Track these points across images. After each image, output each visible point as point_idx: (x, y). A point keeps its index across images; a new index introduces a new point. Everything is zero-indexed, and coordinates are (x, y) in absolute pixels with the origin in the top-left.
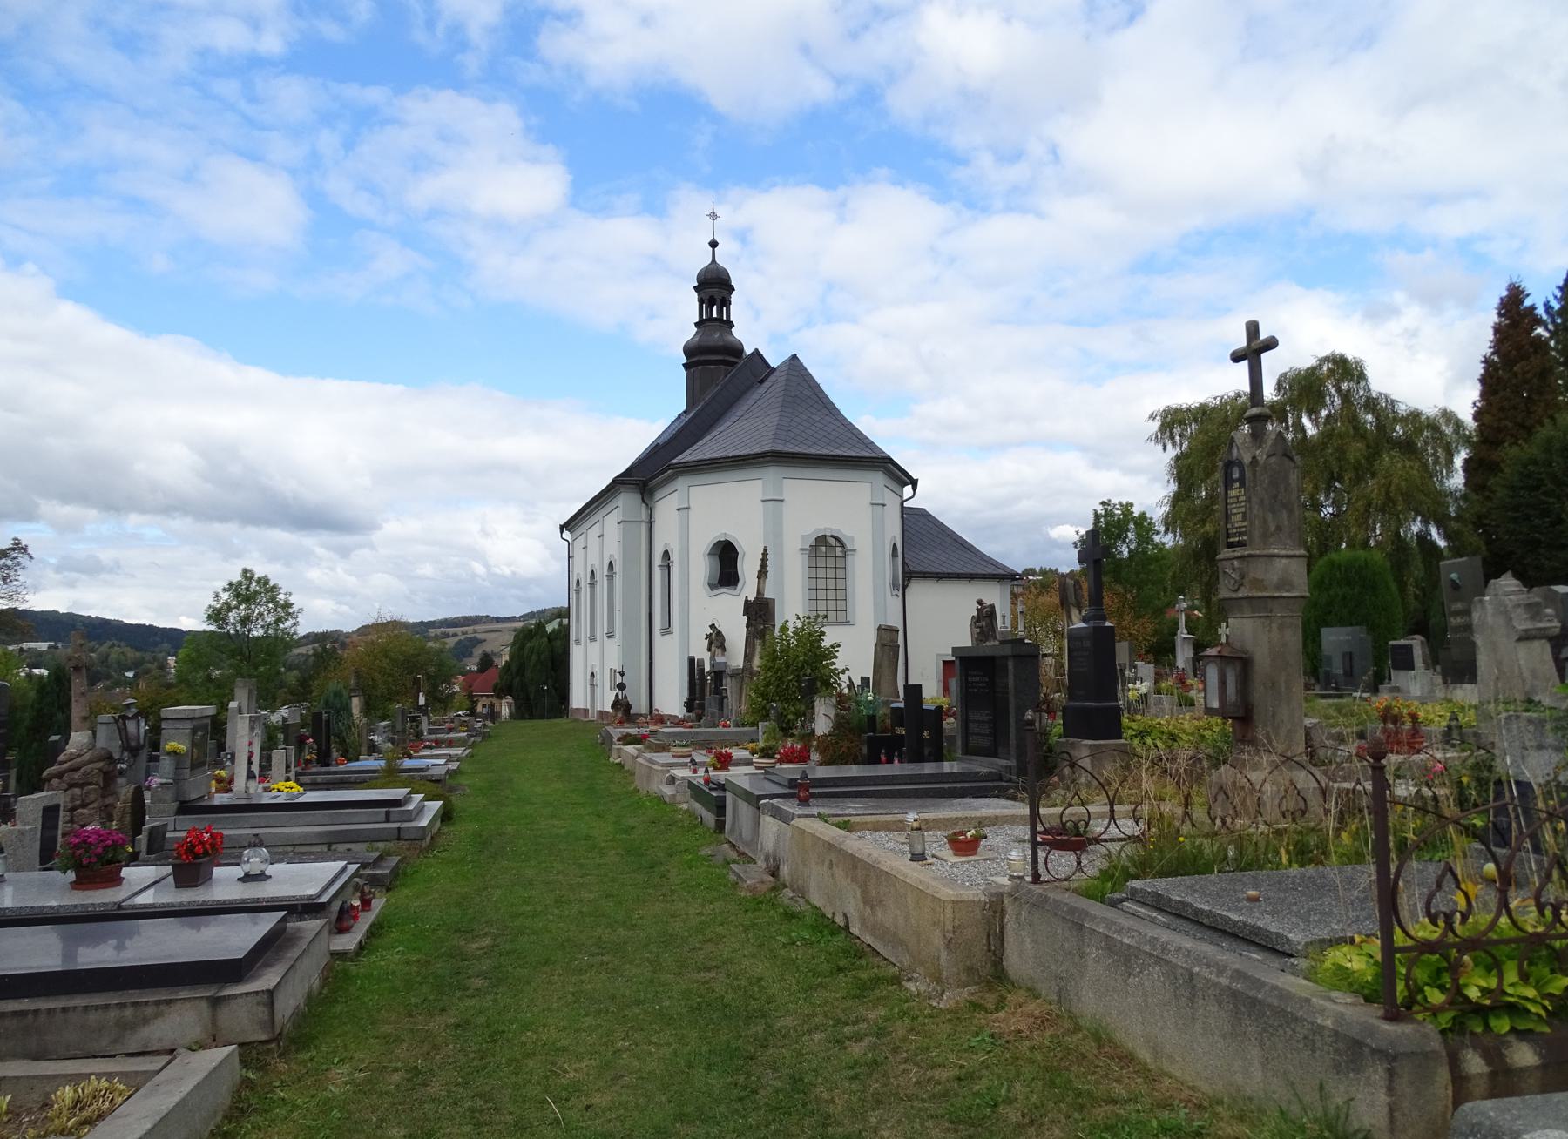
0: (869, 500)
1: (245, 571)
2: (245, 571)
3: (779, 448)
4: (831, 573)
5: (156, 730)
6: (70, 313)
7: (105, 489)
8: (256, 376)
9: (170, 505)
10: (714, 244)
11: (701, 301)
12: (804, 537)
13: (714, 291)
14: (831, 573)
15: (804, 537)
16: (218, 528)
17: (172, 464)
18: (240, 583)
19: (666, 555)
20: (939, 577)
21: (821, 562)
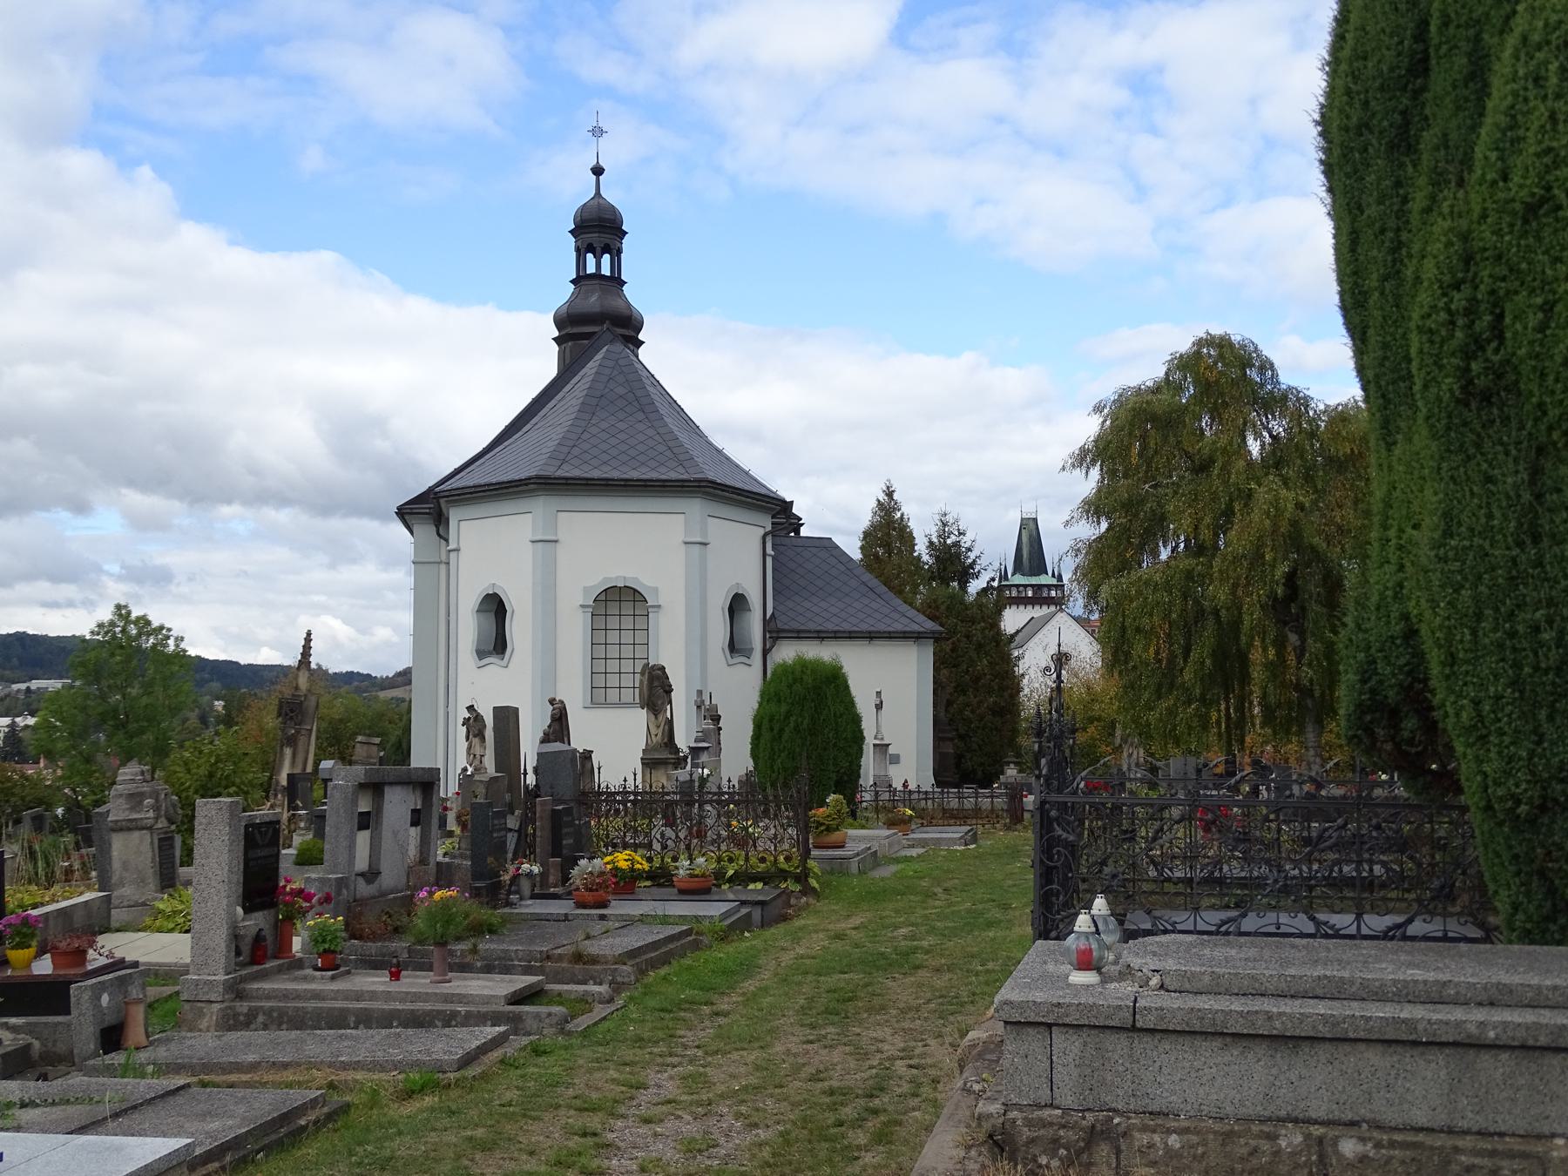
0: (681, 538)
1: (119, 607)
2: (119, 607)
3: (550, 471)
4: (627, 637)
5: (1530, 759)
6: (195, 237)
7: (189, 475)
8: (419, 309)
9: (267, 494)
10: (598, 171)
11: (578, 250)
12: (586, 590)
13: (593, 237)
14: (627, 637)
15: (586, 590)
16: (336, 524)
17: (288, 436)
18: (112, 624)
19: (495, 607)
20: (871, 636)
21: (613, 622)
